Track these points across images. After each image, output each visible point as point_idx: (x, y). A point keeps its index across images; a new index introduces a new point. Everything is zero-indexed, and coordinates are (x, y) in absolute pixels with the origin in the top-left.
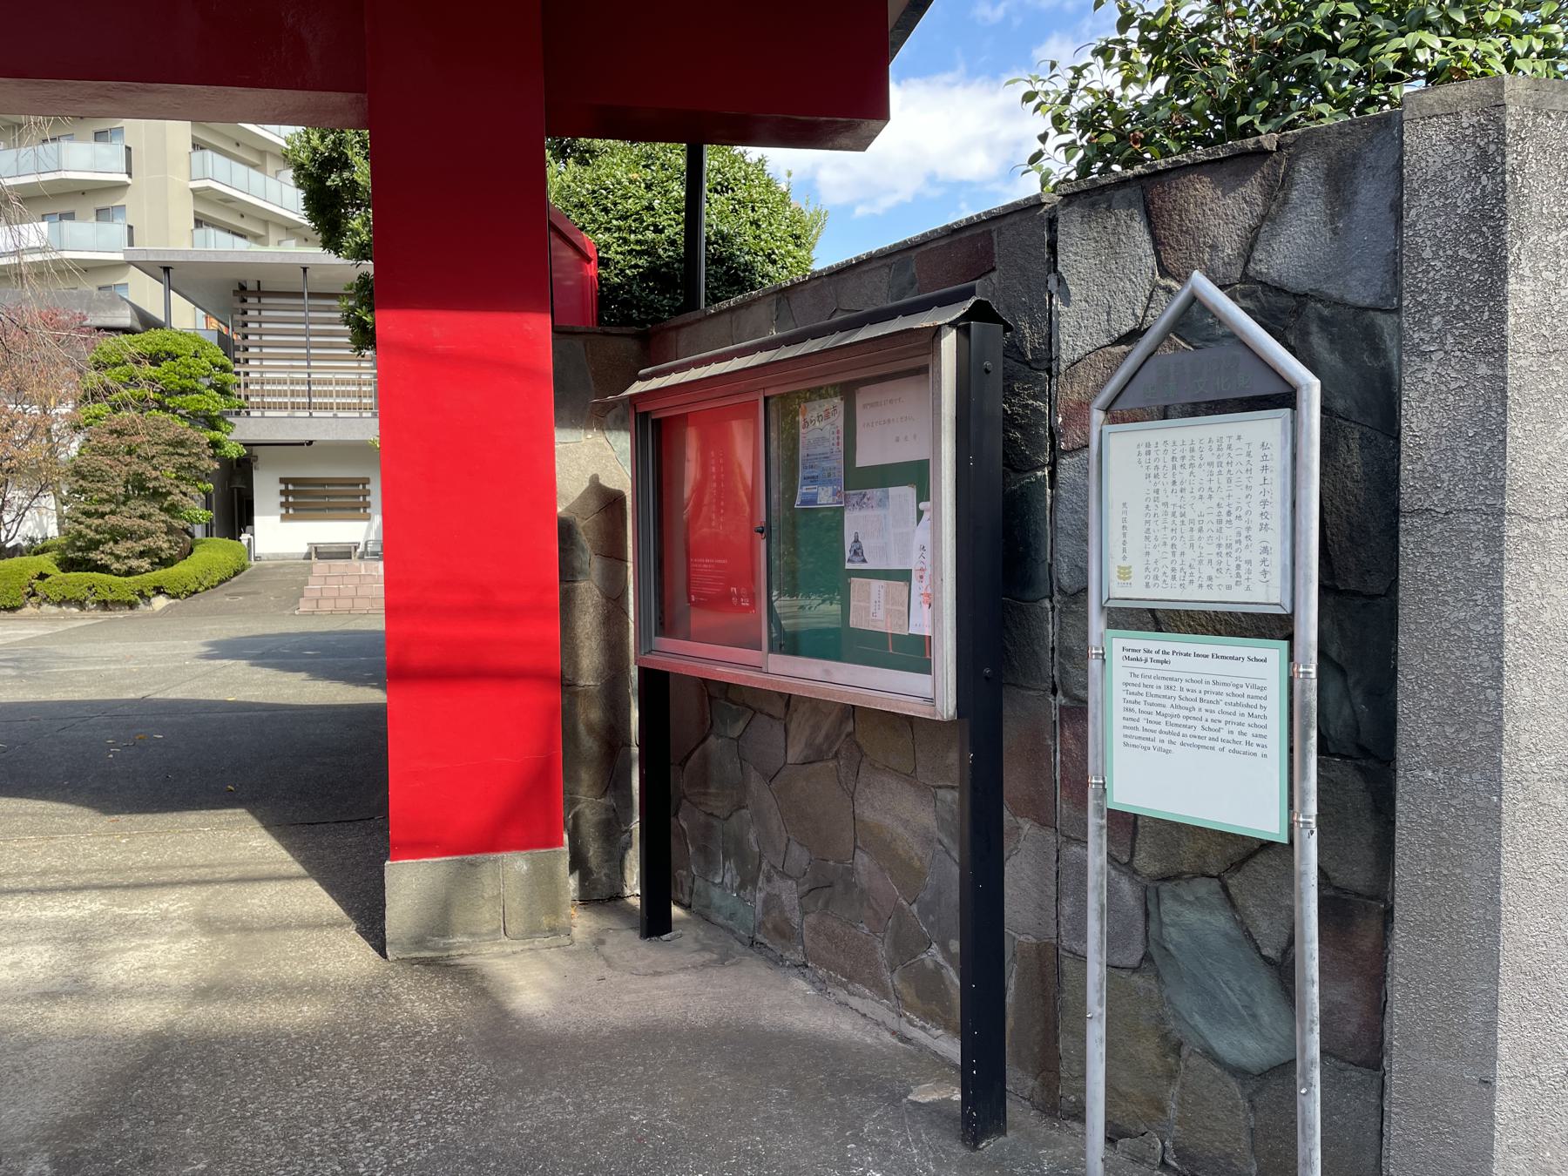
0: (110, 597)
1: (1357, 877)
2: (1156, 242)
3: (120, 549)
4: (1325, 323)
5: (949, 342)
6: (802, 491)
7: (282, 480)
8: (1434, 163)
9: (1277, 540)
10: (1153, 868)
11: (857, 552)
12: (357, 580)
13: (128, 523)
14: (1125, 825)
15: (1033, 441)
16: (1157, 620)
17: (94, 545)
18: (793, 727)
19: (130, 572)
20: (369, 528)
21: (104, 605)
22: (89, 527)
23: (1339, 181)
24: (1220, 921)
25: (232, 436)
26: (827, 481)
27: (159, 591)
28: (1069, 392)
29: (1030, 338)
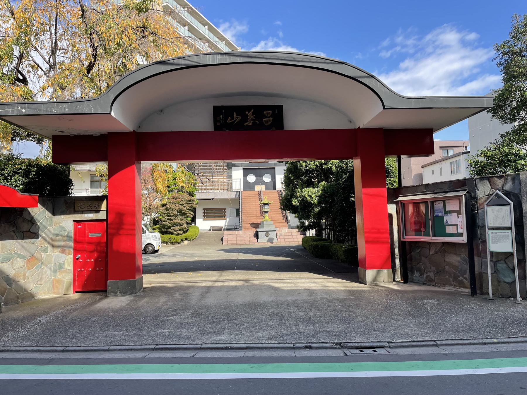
0: (174, 241)
1: (521, 258)
2: (490, 183)
3: (176, 228)
4: (513, 195)
5: (464, 196)
6: (435, 214)
7: (203, 209)
8: (524, 179)
9: (509, 219)
10: (495, 260)
11: (447, 222)
13: (178, 222)
14: (492, 253)
15: (475, 208)
16: (493, 229)
17: (169, 227)
18: (431, 249)
19: (178, 234)
21: (172, 243)
23: (513, 179)
24: (505, 265)
26: (440, 212)
27: (186, 239)
28: (480, 202)
29: (473, 195)
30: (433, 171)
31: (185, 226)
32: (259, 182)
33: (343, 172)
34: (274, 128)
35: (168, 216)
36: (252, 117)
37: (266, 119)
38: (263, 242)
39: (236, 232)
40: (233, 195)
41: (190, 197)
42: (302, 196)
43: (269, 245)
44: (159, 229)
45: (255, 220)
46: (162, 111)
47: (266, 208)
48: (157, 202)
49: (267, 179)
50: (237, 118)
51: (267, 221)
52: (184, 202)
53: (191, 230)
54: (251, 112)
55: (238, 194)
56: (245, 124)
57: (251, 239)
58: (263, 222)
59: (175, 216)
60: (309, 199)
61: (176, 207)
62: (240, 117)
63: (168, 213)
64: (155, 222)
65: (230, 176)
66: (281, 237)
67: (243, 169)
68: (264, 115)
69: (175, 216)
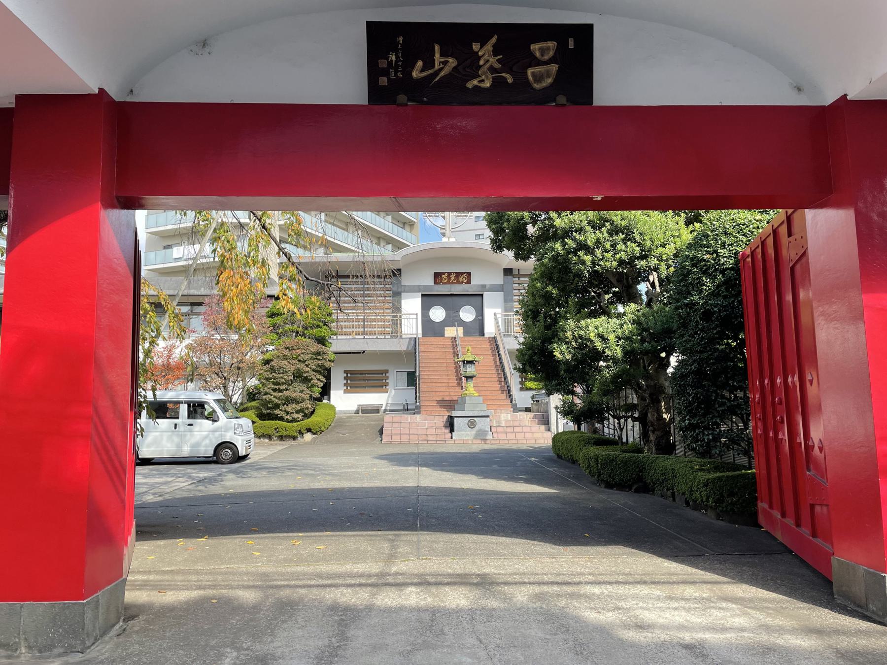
0: (285, 433)
3: (289, 408)
12: (407, 425)
13: (294, 395)
17: (277, 406)
19: (294, 420)
20: (389, 396)
21: (281, 438)
22: (275, 397)
25: (331, 349)
27: (309, 430)
30: (176, 425)
31: (308, 404)
32: (452, 320)
33: (705, 273)
34: (562, 99)
35: (274, 384)
36: (493, 61)
37: (538, 69)
38: (465, 440)
39: (408, 417)
40: (401, 346)
41: (320, 346)
42: (581, 337)
43: (477, 447)
44: (257, 408)
45: (447, 394)
46: (204, 44)
47: (470, 370)
48: (254, 356)
49: (467, 314)
50: (444, 64)
51: (471, 395)
52: (307, 357)
53: (320, 411)
54: (489, 47)
55: (412, 342)
56: (470, 85)
57: (439, 431)
58: (463, 398)
59: (287, 383)
60: (599, 345)
61: (290, 367)
62: (452, 62)
63: (275, 379)
64: (252, 395)
65: (397, 309)
66: (499, 430)
67: (423, 295)
68: (532, 55)
69: (289, 383)
